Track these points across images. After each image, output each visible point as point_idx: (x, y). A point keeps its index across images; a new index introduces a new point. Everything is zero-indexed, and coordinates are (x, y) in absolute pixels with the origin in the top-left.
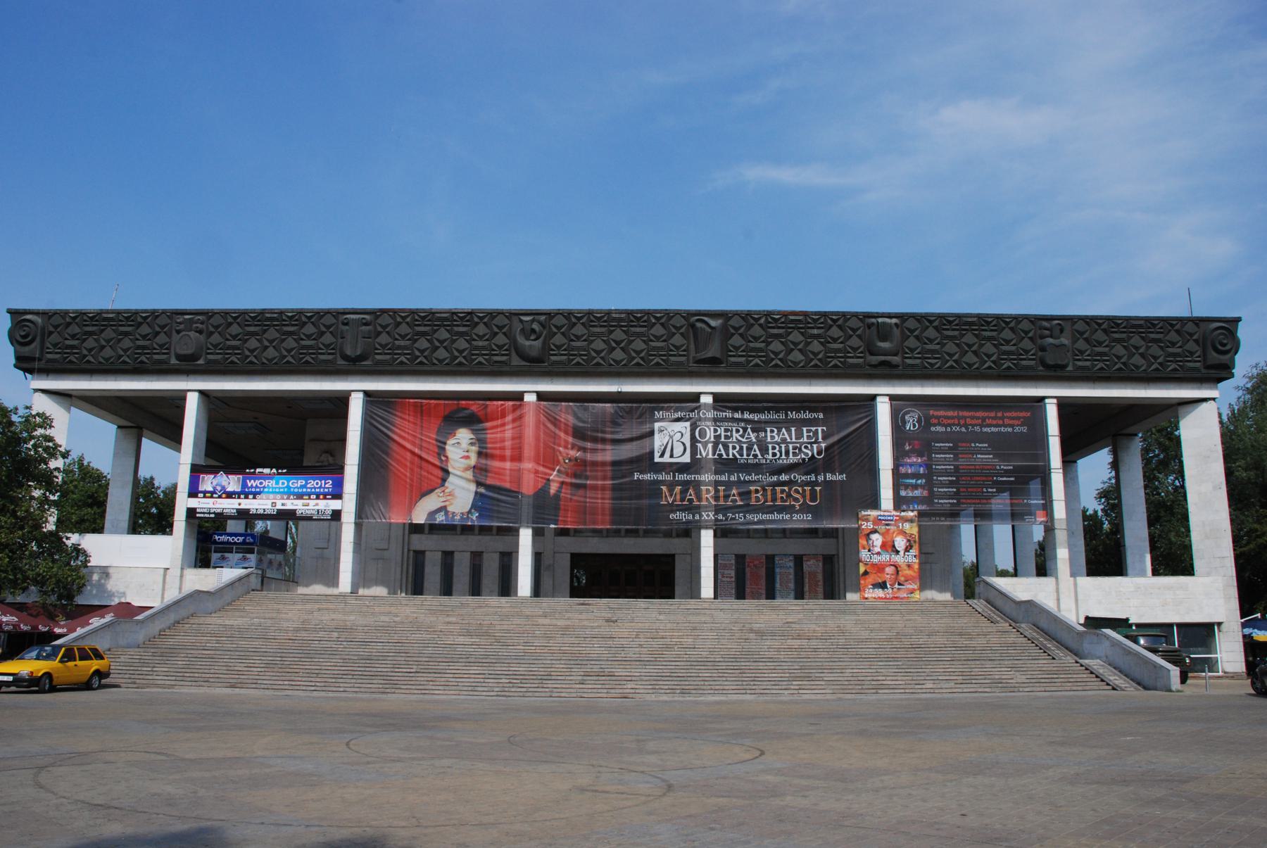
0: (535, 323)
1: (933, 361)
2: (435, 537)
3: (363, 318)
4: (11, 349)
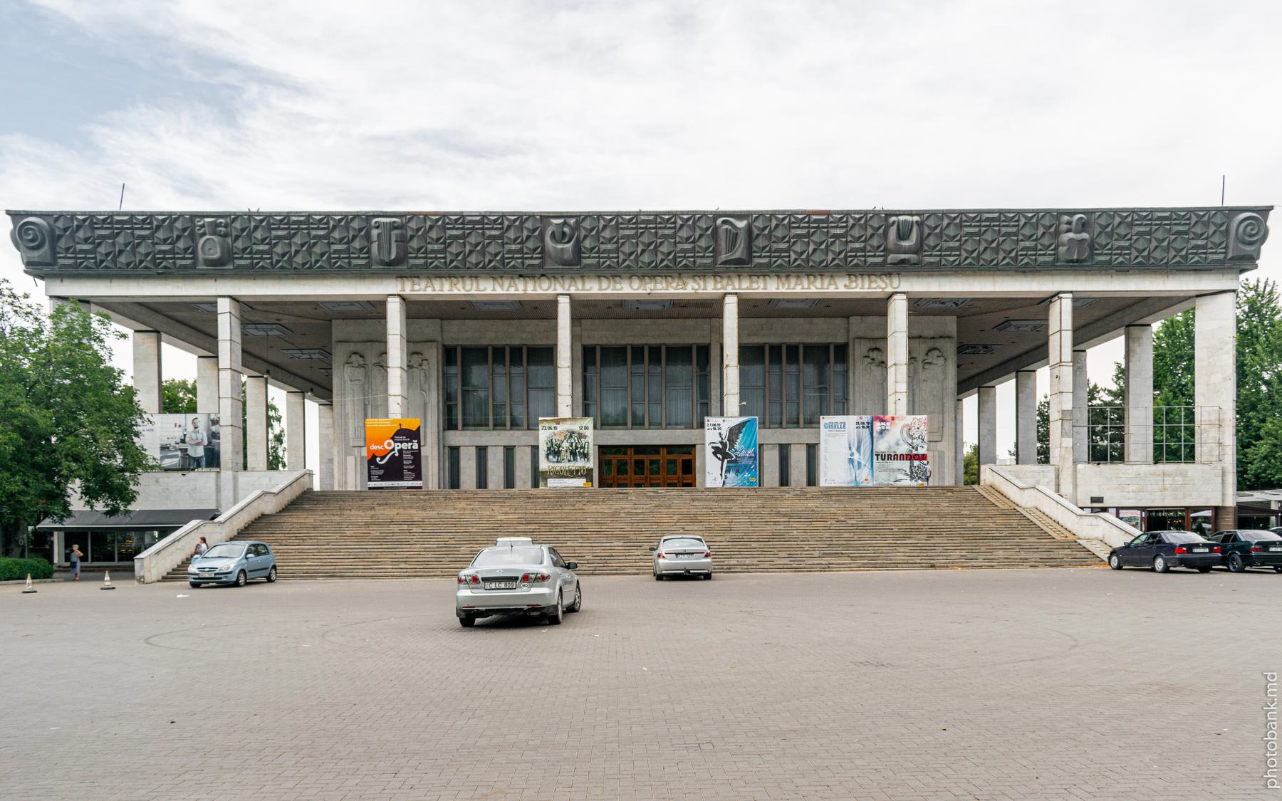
1: (952, 259)
2: (468, 433)
3: (394, 222)
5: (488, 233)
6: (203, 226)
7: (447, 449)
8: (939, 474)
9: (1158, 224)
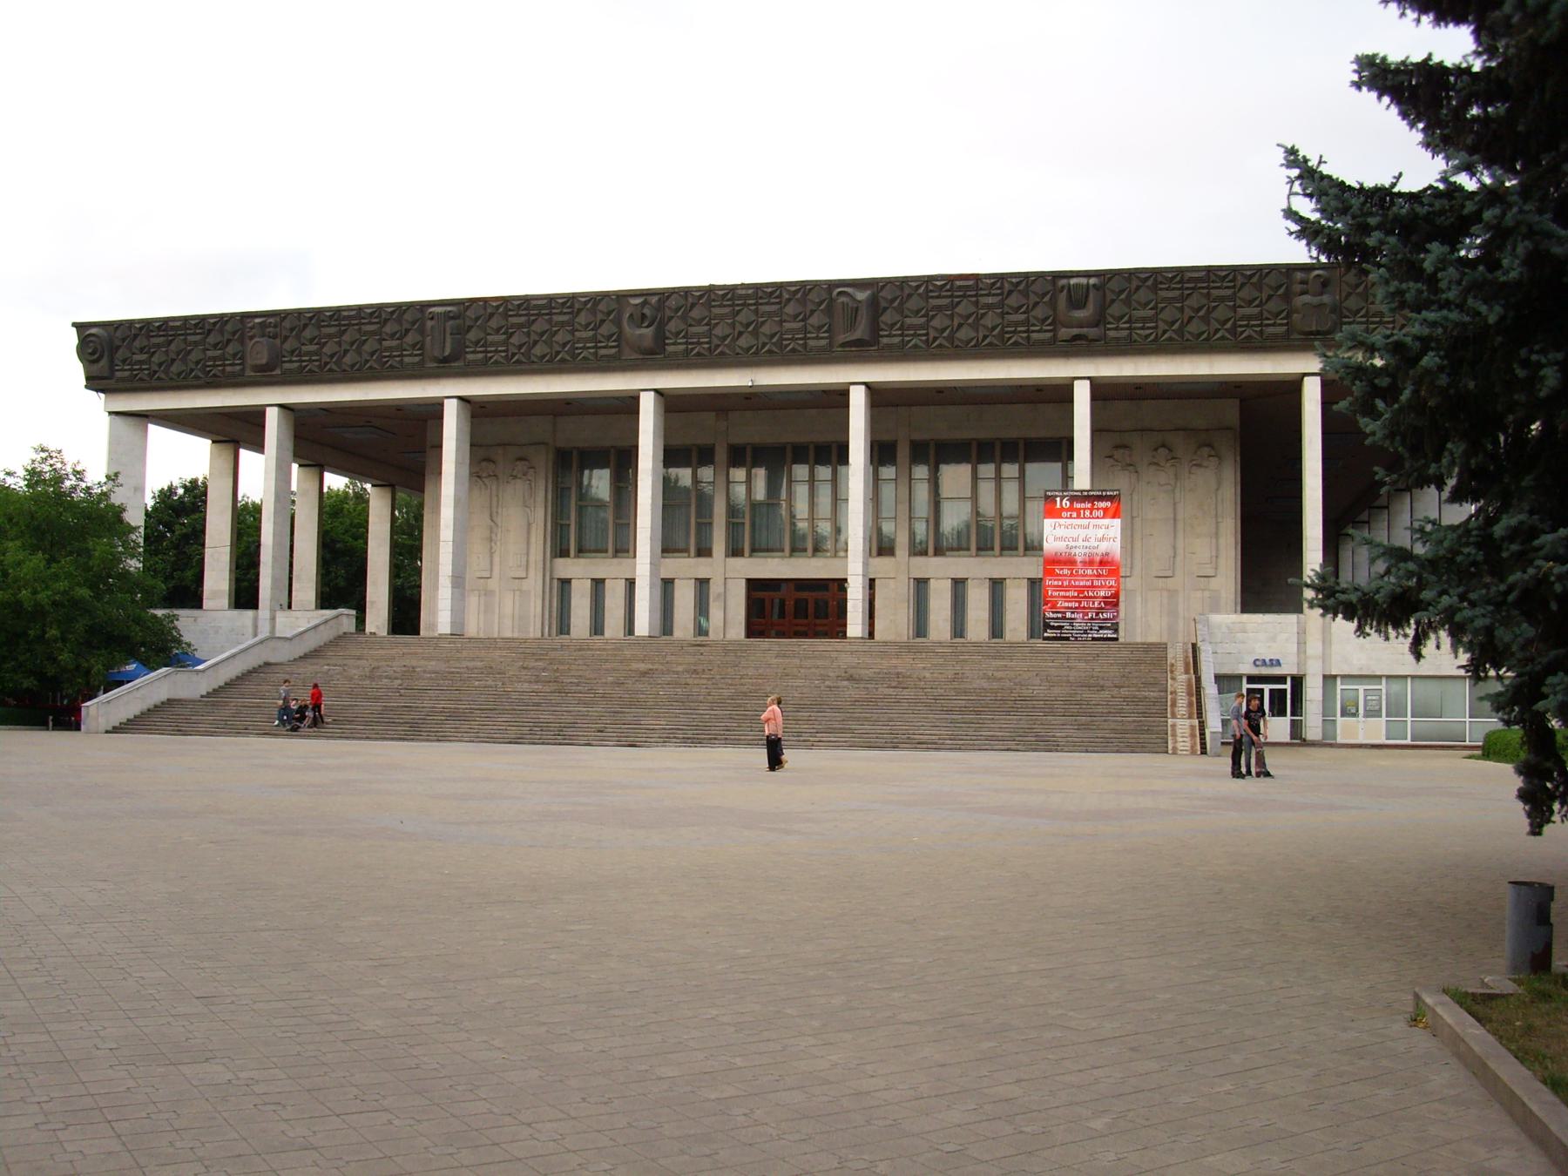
0: (647, 306)
2: (582, 561)
3: (450, 312)
4: (80, 366)
5: (1215, 293)
6: (252, 328)
7: (555, 582)
9: (1192, 288)
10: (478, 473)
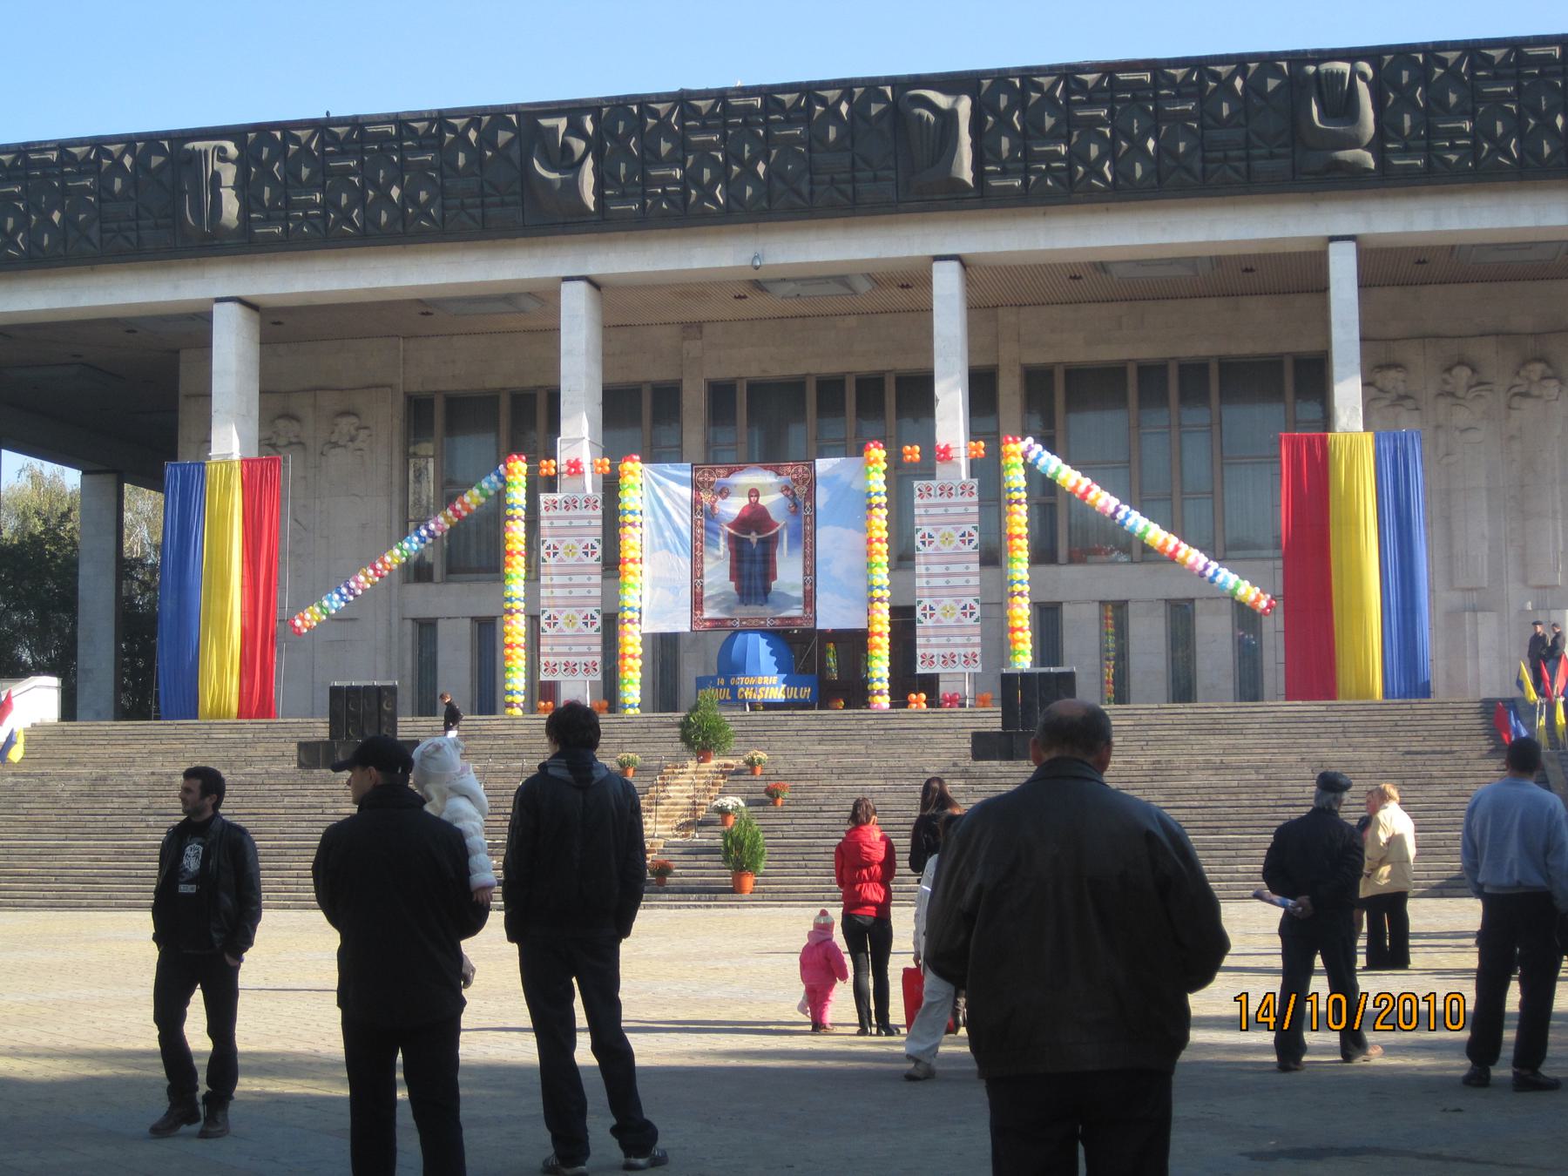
2: (454, 587)
8: (60, 775)
10: (269, 439)
